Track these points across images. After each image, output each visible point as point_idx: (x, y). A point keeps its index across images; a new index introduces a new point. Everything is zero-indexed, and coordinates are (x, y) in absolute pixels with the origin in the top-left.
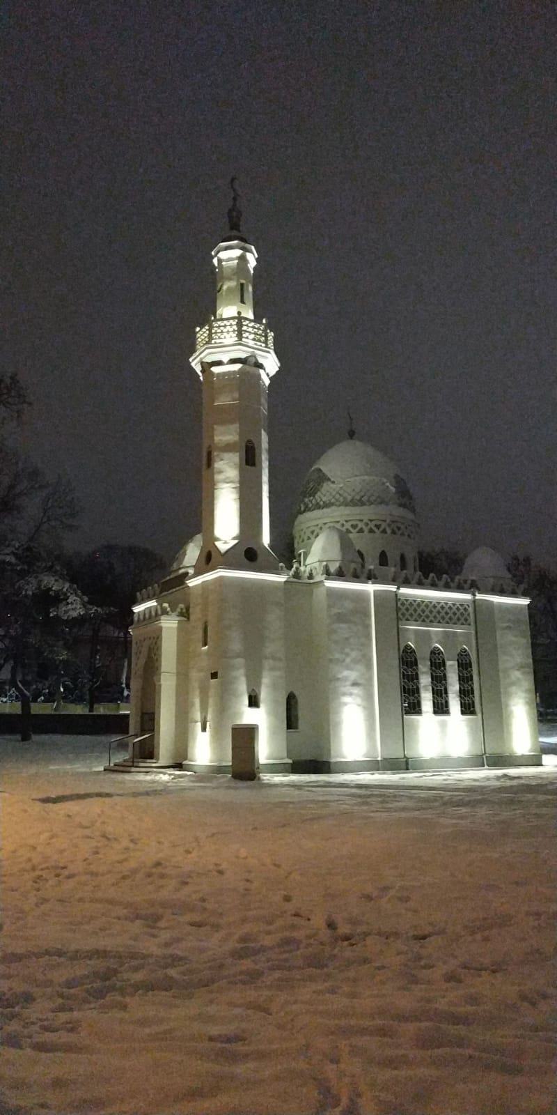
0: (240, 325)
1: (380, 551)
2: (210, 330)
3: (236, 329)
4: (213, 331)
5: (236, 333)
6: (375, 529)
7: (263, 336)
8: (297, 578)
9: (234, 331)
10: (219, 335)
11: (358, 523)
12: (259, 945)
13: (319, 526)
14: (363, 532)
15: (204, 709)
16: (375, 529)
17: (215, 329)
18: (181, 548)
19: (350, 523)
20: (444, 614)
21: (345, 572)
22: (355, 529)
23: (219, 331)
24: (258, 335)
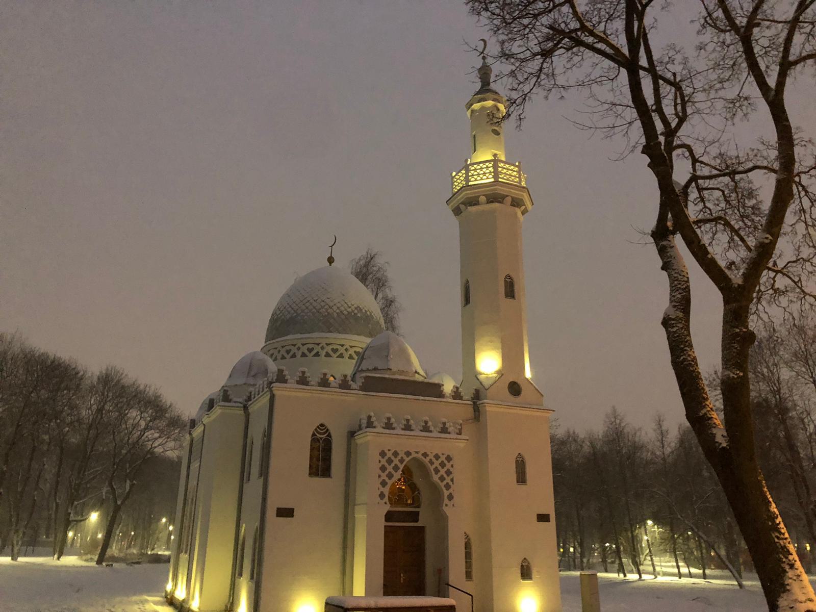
0: (495, 167)
1: (523, 393)
2: (467, 173)
3: (492, 171)
4: (470, 174)
5: (493, 174)
6: (307, 353)
7: (517, 177)
8: (324, 386)
9: (490, 172)
10: (475, 177)
11: (292, 347)
12: (90, 505)
13: (297, 346)
14: (343, 357)
15: (182, 578)
16: (307, 353)
17: (472, 172)
18: (503, 349)
19: (306, 347)
20: (444, 460)
21: (288, 377)
22: (335, 353)
23: (476, 173)
24: (512, 176)
